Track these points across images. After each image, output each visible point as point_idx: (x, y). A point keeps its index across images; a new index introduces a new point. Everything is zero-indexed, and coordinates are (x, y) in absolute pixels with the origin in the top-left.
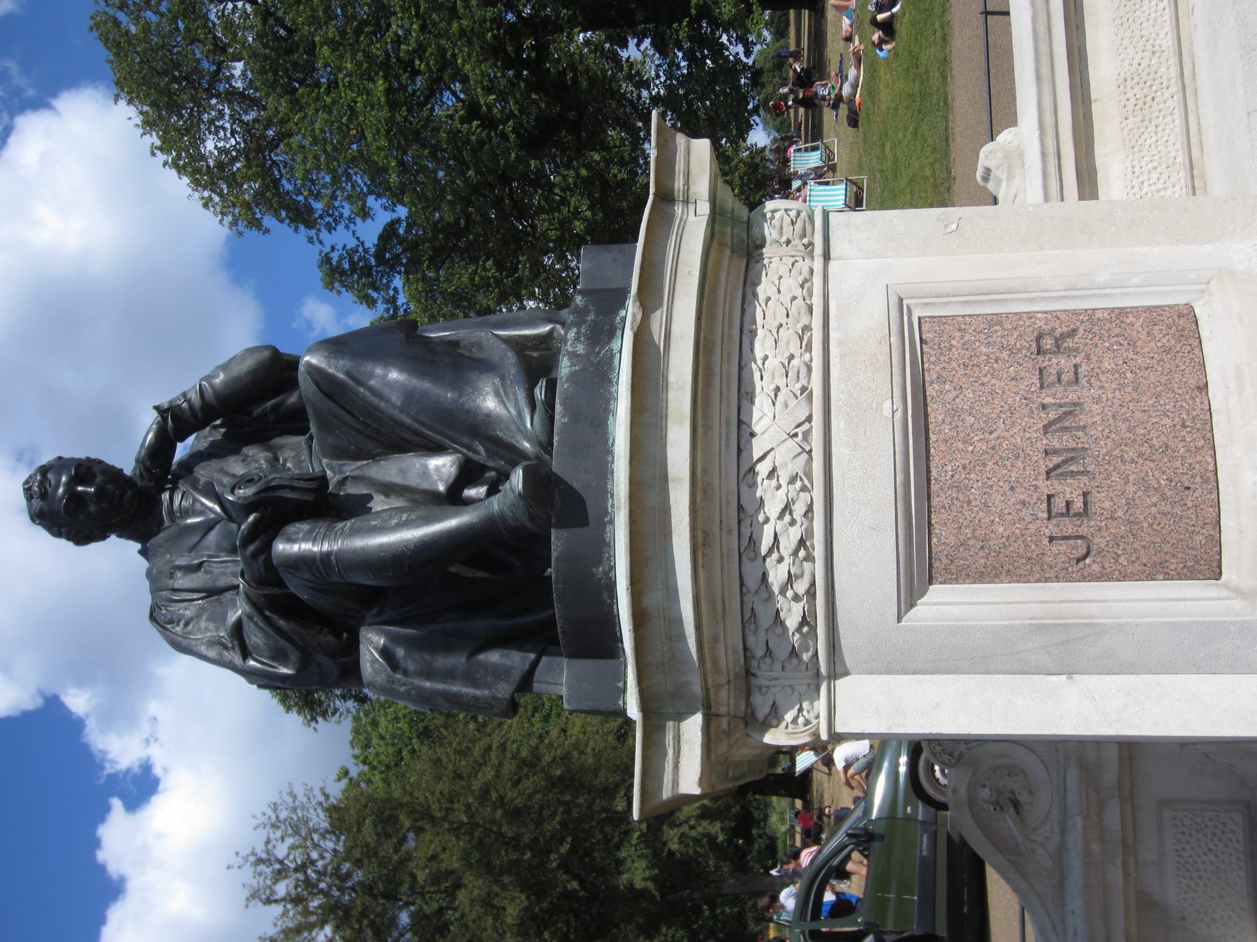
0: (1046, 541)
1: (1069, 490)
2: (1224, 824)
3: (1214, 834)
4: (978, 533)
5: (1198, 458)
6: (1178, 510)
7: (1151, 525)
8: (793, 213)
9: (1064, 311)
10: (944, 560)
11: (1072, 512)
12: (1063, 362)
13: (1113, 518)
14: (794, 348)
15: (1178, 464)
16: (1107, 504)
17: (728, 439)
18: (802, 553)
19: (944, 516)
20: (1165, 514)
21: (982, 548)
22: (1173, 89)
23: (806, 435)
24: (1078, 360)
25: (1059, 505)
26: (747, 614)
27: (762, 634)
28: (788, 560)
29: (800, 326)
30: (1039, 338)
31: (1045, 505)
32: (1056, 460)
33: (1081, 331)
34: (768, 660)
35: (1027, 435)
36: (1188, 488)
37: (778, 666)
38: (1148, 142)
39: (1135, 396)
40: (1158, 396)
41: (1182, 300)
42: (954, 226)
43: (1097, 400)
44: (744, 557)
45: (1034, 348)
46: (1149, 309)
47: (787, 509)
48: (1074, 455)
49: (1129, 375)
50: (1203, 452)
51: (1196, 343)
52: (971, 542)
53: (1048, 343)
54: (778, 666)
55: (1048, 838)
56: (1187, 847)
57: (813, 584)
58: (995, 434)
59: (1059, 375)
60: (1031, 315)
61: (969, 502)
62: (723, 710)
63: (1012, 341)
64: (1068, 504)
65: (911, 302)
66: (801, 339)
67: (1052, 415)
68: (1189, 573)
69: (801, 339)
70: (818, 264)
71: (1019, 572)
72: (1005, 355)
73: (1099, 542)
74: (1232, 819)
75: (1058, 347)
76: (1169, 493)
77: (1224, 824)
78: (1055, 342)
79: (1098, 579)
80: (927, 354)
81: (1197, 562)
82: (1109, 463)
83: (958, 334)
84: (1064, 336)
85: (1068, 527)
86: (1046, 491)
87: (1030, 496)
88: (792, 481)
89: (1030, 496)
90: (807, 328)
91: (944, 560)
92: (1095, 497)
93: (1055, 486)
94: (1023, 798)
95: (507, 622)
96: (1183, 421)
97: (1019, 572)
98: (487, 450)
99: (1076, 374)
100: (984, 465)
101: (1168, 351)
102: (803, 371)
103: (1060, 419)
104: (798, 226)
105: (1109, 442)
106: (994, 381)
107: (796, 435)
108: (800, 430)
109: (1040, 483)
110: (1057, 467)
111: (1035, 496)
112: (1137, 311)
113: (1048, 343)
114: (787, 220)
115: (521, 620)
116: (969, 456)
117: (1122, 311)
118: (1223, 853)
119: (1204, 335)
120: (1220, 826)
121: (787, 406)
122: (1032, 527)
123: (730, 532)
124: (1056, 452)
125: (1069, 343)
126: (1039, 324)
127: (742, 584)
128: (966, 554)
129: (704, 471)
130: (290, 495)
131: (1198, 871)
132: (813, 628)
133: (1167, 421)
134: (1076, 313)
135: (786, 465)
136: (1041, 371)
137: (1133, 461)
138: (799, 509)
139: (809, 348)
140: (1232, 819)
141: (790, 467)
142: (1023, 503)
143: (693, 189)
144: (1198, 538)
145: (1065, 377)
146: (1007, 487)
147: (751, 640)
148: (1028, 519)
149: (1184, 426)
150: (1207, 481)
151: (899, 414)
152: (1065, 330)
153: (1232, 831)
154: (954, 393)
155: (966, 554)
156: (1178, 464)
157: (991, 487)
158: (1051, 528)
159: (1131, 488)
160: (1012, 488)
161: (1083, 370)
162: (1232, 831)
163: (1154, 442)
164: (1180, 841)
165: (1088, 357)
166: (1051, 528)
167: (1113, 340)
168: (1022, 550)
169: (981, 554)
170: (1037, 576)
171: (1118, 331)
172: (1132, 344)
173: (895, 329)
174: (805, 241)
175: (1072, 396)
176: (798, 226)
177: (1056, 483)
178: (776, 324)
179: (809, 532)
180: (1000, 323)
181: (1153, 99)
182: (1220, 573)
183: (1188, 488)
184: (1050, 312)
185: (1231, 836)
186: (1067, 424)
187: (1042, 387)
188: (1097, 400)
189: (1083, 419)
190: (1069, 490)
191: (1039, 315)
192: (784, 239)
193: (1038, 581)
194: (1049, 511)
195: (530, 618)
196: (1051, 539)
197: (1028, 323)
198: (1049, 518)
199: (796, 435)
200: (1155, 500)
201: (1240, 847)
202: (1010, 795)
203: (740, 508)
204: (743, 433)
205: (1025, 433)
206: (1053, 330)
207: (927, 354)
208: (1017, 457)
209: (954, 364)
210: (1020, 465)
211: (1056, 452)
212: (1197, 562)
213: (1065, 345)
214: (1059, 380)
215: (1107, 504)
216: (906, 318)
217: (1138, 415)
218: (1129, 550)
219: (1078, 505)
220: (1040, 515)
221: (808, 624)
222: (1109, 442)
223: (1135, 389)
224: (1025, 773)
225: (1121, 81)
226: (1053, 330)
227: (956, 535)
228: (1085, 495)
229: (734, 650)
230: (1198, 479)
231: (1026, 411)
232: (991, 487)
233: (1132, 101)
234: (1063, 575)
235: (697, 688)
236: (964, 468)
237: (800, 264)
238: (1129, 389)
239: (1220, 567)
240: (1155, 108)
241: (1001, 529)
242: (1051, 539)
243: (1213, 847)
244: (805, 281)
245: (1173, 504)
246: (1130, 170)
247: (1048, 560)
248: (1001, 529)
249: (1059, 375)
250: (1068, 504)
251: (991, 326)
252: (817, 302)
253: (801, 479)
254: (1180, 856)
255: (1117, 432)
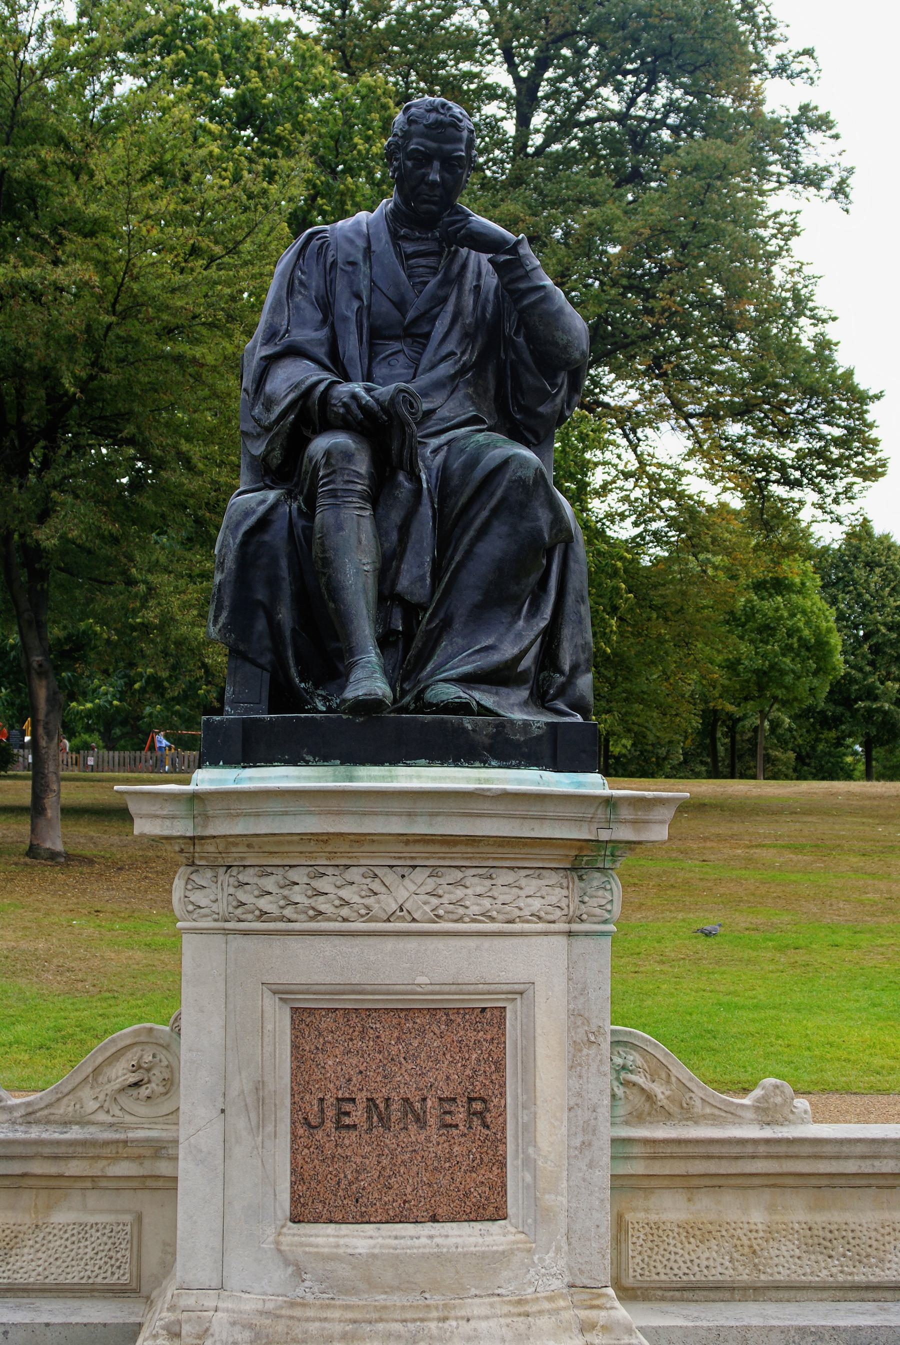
0: (321, 1096)
1: (358, 1115)
2: (119, 1267)
3: (111, 1258)
4: (328, 1045)
5: (380, 1211)
6: (341, 1193)
7: (330, 1173)
8: (609, 907)
9: (505, 1121)
10: (308, 1020)
11: (342, 1117)
12: (460, 1116)
13: (336, 1146)
14: (475, 909)
15: (376, 1195)
16: (347, 1142)
17: (400, 858)
18: (311, 913)
19: (341, 1020)
20: (338, 1183)
21: (317, 1048)
22: (841, 1278)
23: (402, 919)
24: (461, 1128)
25: (348, 1107)
26: (269, 870)
27: (256, 880)
28: (307, 901)
29: (494, 914)
30: (484, 1100)
31: (347, 1096)
32: (382, 1106)
33: (487, 1132)
34: (236, 884)
35: (402, 1086)
36: (357, 1201)
37: (232, 890)
38: (784, 1248)
39: (431, 1168)
40: (430, 1185)
41: (511, 1211)
42: (593, 1039)
43: (428, 1139)
44: (310, 869)
45: (472, 1095)
46: (504, 1185)
47: (346, 903)
48: (385, 1121)
49: (447, 1165)
50: (385, 1215)
51: (471, 1216)
52: (321, 1040)
53: (478, 1106)
54: (232, 890)
55: (108, 1112)
56: (99, 1234)
57: (290, 921)
58: (403, 1062)
59: (450, 1113)
60: (503, 1095)
61: (351, 1040)
62: (198, 849)
63: (481, 1079)
64: (348, 1114)
65: (519, 1001)
66: (482, 915)
67: (417, 1105)
68: (296, 1199)
69: (482, 915)
70: (564, 927)
71: (299, 1075)
72: (468, 1072)
73: (320, 1134)
74: (123, 1275)
75: (474, 1114)
76: (354, 1187)
77: (119, 1267)
78: (480, 1110)
79: (293, 1133)
80: (479, 1025)
81: (303, 1205)
82: (378, 1145)
83: (489, 1037)
84: (483, 1119)
85: (330, 1113)
86: (359, 1097)
87: (355, 1086)
88: (367, 908)
89: (355, 1086)
90: (493, 919)
91: (308, 1020)
92: (354, 1134)
93: (361, 1105)
94: (144, 1091)
95: (288, 640)
96: (409, 1202)
97: (299, 1075)
98: (432, 630)
99: (451, 1126)
100: (380, 1052)
101: (466, 1195)
102: (455, 917)
103: (413, 1111)
104: (598, 911)
105: (395, 1146)
106: (446, 1063)
107: (402, 910)
108: (405, 913)
109: (364, 1093)
110: (376, 1106)
111: (355, 1089)
112: (503, 1177)
113: (478, 1106)
114: (603, 902)
115: (290, 653)
116: (387, 1041)
117: (503, 1165)
118: (95, 1265)
119: (478, 1226)
120: (118, 1264)
121: (425, 903)
122: (331, 1086)
123: (329, 859)
124: (387, 1106)
125: (476, 1122)
126: (496, 1101)
127: (291, 866)
128: (313, 1036)
129: (373, 841)
130: (395, 446)
131: (79, 1242)
132: (312, 919)
133: (409, 1190)
134: (504, 1129)
135: (379, 903)
136: (454, 1099)
137: (379, 1162)
138: (345, 912)
139: (474, 921)
140: (123, 1275)
141: (377, 905)
142: (350, 1080)
143: (623, 827)
144: (320, 1206)
145: (448, 1117)
146: (362, 1068)
147: (251, 871)
148: (337, 1083)
149: (405, 1202)
150: (362, 1216)
151: (419, 989)
152: (489, 1120)
153: (113, 1274)
154: (438, 1032)
155: (313, 1036)
156: (376, 1195)
157: (363, 1057)
158: (330, 1100)
159: (359, 1160)
160: (361, 1072)
161: (455, 1132)
162: (113, 1274)
163: (393, 1179)
164: (105, 1228)
165: (464, 1135)
166: (330, 1100)
167: (478, 1156)
168: (314, 1077)
169: (313, 1047)
170: (296, 1088)
171: (486, 1159)
172: (473, 1170)
173: (493, 987)
174: (584, 917)
175: (432, 1121)
176: (598, 911)
177: (365, 1105)
178: (496, 894)
179: (329, 920)
180: (497, 1070)
181: (830, 1257)
182: (294, 1222)
183: (357, 1201)
184: (505, 1110)
185: (109, 1273)
186: (410, 1116)
187: (440, 1099)
188: (428, 1139)
189: (413, 1128)
190: (358, 1115)
191: (503, 1101)
192: (586, 899)
193: (292, 1089)
194: (343, 1100)
195: (291, 662)
196: (322, 1100)
197: (496, 1092)
198: (337, 1099)
199: (402, 910)
200: (349, 1177)
201: (99, 1280)
202: (146, 1080)
203: (348, 867)
204: (406, 869)
205: (405, 1083)
206: (489, 1111)
207: (479, 1025)
208: (385, 1077)
209: (462, 1033)
210: (379, 1079)
211: (387, 1106)
212: (303, 1205)
213: (475, 1119)
214: (445, 1113)
215: (347, 1142)
216: (503, 996)
217: (415, 1169)
218: (314, 1156)
219: (347, 1121)
220: (340, 1092)
221: (261, 916)
222: (395, 1146)
223: (436, 1168)
224: (166, 1093)
225: (853, 1226)
226: (489, 1111)
227: (327, 1029)
228: (354, 1126)
229: (243, 858)
230: (363, 1209)
231: (421, 1085)
232: (363, 1057)
233: (829, 1236)
234: (295, 1107)
235: (210, 832)
236: (378, 1037)
237: (558, 913)
238: (436, 1164)
239: (299, 1222)
240: (820, 1258)
241: (330, 1063)
242: (322, 1100)
243: (100, 1255)
244: (539, 918)
245: (346, 1190)
246: (753, 1227)
247: (307, 1097)
248: (330, 1063)
249: (450, 1113)
250: (348, 1114)
251: (495, 1063)
252: (517, 927)
253: (368, 915)
254: (92, 1227)
255: (402, 1153)
